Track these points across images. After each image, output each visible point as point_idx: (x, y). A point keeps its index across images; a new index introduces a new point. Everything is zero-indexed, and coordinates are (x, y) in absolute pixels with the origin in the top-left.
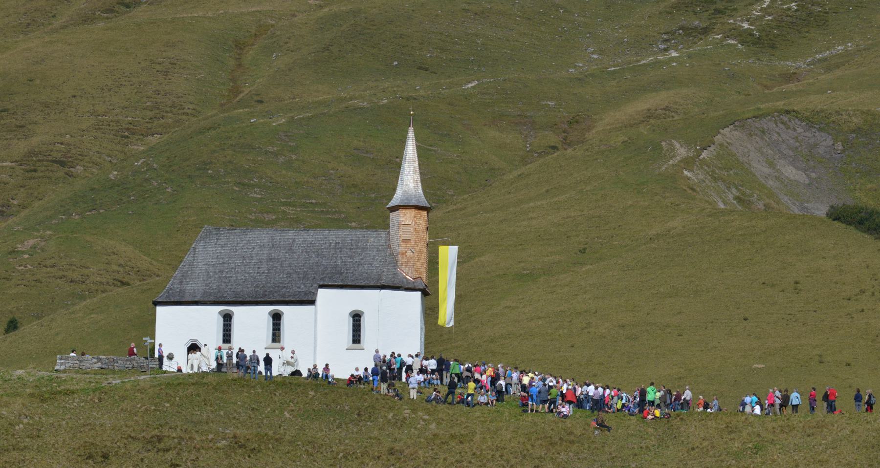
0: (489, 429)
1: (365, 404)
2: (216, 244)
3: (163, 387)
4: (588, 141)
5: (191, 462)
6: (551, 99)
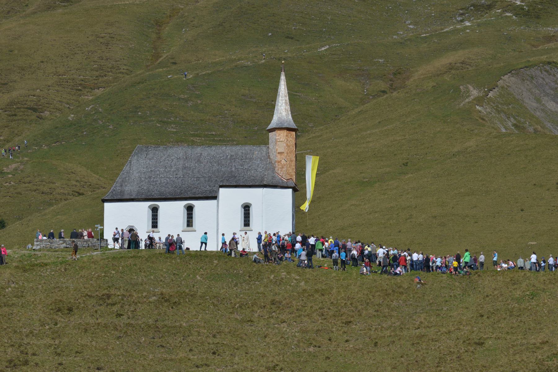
0: (342, 285)
1: (254, 269)
2: (146, 158)
3: (110, 260)
4: (407, 86)
5: (131, 312)
6: (381, 57)
